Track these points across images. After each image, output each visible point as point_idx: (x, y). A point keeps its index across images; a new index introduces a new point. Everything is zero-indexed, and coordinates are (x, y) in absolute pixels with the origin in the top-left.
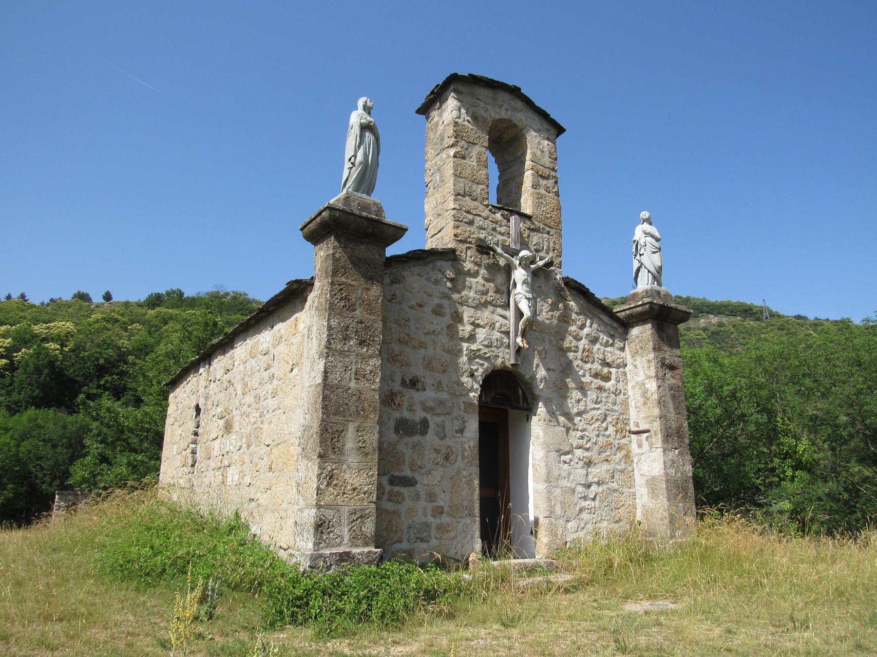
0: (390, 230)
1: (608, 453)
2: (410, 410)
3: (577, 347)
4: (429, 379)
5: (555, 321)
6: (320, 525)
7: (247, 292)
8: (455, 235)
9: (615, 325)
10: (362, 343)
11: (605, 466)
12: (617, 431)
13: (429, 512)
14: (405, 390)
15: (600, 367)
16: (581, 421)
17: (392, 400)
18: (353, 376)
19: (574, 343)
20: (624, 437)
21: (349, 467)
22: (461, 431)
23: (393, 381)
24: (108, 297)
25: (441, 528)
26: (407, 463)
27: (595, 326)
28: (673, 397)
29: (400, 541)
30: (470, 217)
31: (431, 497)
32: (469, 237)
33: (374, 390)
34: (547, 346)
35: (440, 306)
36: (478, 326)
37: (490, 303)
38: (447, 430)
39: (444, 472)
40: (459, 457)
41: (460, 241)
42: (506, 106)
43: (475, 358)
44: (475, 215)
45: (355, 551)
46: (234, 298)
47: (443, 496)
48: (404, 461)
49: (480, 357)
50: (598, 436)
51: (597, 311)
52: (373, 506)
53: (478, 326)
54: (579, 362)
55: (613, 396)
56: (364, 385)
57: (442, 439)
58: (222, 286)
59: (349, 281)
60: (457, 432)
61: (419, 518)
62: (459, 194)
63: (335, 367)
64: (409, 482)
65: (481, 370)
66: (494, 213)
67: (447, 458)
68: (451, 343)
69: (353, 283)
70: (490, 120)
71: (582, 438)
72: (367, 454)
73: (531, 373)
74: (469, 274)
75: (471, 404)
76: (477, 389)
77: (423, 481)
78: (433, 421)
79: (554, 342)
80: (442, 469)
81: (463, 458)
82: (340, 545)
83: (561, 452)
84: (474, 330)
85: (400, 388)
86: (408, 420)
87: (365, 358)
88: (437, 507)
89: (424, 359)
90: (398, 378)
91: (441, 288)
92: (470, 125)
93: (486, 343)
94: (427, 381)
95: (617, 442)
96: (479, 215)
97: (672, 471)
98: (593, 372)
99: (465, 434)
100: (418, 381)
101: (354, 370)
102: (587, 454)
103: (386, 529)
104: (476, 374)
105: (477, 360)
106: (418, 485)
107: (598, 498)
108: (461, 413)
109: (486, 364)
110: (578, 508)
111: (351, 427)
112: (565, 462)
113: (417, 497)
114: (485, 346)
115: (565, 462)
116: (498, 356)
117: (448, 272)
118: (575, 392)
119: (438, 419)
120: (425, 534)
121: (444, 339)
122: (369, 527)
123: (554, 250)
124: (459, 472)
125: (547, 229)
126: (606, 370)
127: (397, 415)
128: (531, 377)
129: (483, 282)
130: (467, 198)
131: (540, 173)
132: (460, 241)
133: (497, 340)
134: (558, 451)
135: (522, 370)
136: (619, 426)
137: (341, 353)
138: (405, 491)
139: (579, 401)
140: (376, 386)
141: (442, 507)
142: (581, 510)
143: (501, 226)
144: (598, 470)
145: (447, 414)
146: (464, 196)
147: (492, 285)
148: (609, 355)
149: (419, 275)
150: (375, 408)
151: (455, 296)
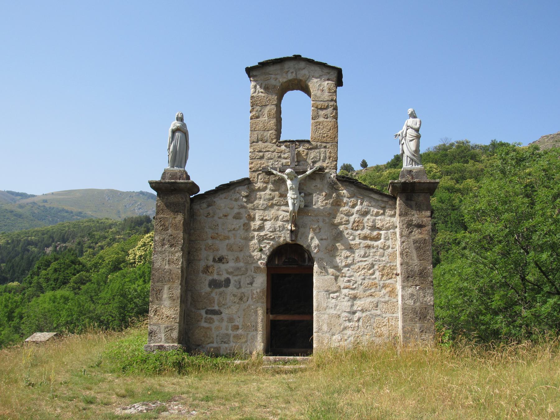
0: (183, 185)
1: (373, 290)
2: (218, 274)
3: (348, 221)
4: (230, 256)
5: (329, 206)
6: (151, 333)
7: (468, 140)
8: (250, 169)
9: (385, 199)
10: (171, 246)
11: (370, 299)
12: (383, 275)
13: (230, 328)
14: (215, 264)
15: (369, 232)
16: (348, 270)
17: (207, 270)
18: (167, 263)
19: (345, 218)
20: (391, 278)
21: (165, 306)
22: (251, 284)
23: (207, 260)
24: (364, 164)
25: (237, 337)
26: (216, 302)
27: (365, 203)
28: (418, 249)
29: (212, 343)
30: (261, 154)
31: (231, 320)
32: (260, 167)
33: (178, 268)
34: (321, 224)
35: (239, 213)
36: (266, 220)
37: (276, 205)
38: (242, 284)
39: (239, 307)
40: (250, 298)
41: (254, 171)
42: (291, 71)
43: (263, 240)
44: (265, 152)
45: (166, 345)
46: (458, 147)
47: (238, 320)
48: (214, 302)
49: (267, 239)
50: (364, 279)
51: (367, 193)
52: (177, 324)
53: (266, 220)
54: (350, 231)
55: (381, 250)
56: (173, 267)
57: (238, 288)
58: (447, 139)
59: (165, 216)
60: (248, 284)
61: (223, 331)
62: (254, 142)
63: (158, 259)
64: (218, 313)
65: (268, 247)
66: (280, 146)
67: (241, 299)
68: (246, 234)
69: (167, 216)
70: (278, 84)
71: (349, 281)
72: (174, 300)
73: (307, 244)
74: (259, 190)
75: (259, 268)
76: (264, 258)
77: (226, 313)
78: (233, 279)
79: (327, 221)
80: (238, 305)
81: (252, 298)
82: (160, 342)
83: (330, 292)
84: (263, 223)
85: (213, 263)
86: (216, 280)
87: (173, 253)
88: (235, 325)
89: (227, 246)
90: (211, 258)
91: (239, 203)
92: (263, 95)
93: (271, 230)
94: (229, 257)
95: (382, 282)
96: (268, 151)
97: (411, 302)
98: (362, 236)
99: (253, 285)
100: (223, 258)
101: (167, 260)
102: (352, 292)
103: (204, 336)
104: (264, 249)
105: (265, 241)
106: (223, 315)
107: (361, 320)
108: (253, 274)
109: (272, 242)
110: (342, 327)
111: (166, 288)
112: (333, 298)
113: (222, 320)
114: (270, 232)
115: (333, 298)
116: (281, 237)
117: (243, 193)
118: (344, 252)
119: (236, 278)
120: (226, 340)
121: (241, 232)
122: (175, 334)
123: (329, 158)
124: (249, 306)
125: (324, 145)
126: (375, 233)
127: (210, 278)
128: (308, 246)
129: (270, 192)
130: (260, 142)
131: (319, 107)
132: (254, 171)
133: (279, 227)
134: (327, 291)
135: (300, 242)
136: (385, 271)
137: (161, 252)
138: (215, 317)
139: (347, 257)
140: (180, 266)
141: (238, 326)
142: (345, 328)
143: (284, 153)
144: (363, 302)
145: (242, 274)
146: (257, 142)
147: (277, 193)
148: (379, 222)
149: (225, 198)
150: (179, 277)
151: (250, 205)
